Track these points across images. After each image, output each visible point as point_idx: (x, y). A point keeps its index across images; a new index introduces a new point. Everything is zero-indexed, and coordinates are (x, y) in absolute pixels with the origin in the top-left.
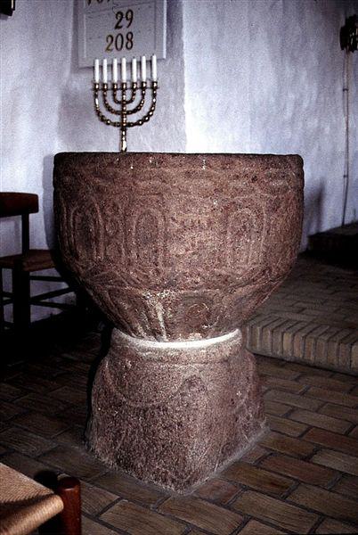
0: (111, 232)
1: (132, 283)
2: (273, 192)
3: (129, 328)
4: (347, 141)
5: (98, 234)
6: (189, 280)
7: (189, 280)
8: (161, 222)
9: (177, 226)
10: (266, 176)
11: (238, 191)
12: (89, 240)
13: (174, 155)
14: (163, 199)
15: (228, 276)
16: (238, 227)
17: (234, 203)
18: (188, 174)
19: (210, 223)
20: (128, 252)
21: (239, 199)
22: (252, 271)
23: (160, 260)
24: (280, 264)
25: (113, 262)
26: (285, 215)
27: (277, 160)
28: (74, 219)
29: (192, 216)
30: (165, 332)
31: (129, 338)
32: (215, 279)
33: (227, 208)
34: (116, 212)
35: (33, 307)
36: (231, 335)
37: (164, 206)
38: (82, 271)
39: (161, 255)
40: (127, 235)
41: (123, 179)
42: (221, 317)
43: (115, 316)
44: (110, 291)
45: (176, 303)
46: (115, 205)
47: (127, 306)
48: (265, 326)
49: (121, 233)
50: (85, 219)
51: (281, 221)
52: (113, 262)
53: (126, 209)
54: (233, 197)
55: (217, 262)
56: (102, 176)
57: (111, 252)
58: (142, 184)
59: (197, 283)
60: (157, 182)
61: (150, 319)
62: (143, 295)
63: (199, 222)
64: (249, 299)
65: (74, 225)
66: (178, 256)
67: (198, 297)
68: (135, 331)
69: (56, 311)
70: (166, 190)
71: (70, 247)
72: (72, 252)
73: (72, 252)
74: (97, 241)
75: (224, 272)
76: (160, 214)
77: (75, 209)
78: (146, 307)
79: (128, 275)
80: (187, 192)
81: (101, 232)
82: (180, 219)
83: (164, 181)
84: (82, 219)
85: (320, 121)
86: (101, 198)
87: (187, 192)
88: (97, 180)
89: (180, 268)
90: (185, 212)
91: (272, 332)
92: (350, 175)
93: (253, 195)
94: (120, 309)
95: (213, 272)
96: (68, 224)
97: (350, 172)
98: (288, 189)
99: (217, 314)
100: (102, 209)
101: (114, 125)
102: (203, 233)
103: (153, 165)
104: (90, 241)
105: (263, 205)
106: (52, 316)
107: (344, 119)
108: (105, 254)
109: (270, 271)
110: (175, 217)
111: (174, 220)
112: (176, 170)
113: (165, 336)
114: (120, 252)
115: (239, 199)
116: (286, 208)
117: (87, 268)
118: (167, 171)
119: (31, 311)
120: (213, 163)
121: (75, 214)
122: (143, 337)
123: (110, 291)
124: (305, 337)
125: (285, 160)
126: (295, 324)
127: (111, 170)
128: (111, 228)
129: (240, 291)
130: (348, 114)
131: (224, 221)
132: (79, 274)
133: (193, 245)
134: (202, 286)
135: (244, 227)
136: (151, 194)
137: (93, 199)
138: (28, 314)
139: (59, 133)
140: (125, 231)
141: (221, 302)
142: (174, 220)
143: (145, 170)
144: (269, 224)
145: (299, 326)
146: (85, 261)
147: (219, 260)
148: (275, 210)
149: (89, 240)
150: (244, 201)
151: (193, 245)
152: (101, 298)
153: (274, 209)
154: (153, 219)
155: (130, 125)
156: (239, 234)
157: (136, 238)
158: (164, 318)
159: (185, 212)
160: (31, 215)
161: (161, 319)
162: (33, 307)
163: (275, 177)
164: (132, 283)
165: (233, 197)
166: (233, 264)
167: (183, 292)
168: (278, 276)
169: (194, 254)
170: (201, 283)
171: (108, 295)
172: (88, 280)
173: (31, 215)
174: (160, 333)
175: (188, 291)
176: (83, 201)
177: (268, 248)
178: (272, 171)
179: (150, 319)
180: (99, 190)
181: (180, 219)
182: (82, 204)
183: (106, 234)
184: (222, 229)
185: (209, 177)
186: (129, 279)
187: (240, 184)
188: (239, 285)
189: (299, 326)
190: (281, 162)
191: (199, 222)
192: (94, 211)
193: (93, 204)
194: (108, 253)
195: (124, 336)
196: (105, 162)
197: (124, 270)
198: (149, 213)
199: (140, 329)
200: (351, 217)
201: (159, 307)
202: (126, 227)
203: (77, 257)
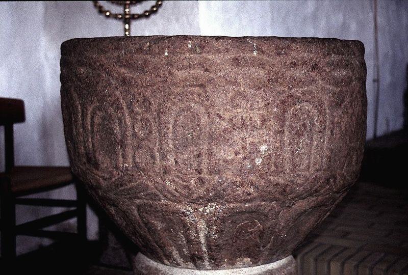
0: (141, 134)
1: (169, 196)
2: (336, 83)
3: (161, 254)
4: (376, 40)
5: (124, 136)
6: (240, 191)
7: (240, 191)
8: (204, 120)
9: (225, 124)
10: (328, 63)
11: (297, 82)
12: (113, 144)
13: (218, 38)
14: (206, 92)
15: (287, 186)
16: (297, 125)
17: (292, 96)
18: (236, 61)
19: (264, 121)
20: (164, 157)
21: (297, 92)
22: (315, 179)
23: (204, 167)
24: (346, 173)
25: (144, 170)
26: (350, 111)
27: (339, 44)
28: (92, 118)
29: (241, 112)
30: (206, 256)
31: (160, 266)
32: (271, 189)
33: (283, 102)
34: (148, 110)
35: (19, 238)
36: (283, 261)
37: (208, 100)
38: (103, 183)
39: (205, 160)
40: (162, 136)
41: (156, 68)
42: (277, 237)
43: (144, 239)
44: (139, 207)
45: (224, 220)
46: (145, 100)
47: (159, 225)
48: (307, 253)
49: (155, 134)
50: (107, 118)
51: (346, 119)
52: (144, 170)
53: (159, 105)
54: (290, 89)
55: (273, 168)
56: (128, 65)
57: (142, 158)
58: (181, 74)
59: (249, 194)
60: (199, 72)
61: (189, 241)
62: (182, 210)
63: (251, 120)
64: (309, 214)
65: (92, 126)
66: (225, 161)
67: (250, 211)
68: (169, 257)
69: (46, 242)
70: (210, 81)
71: (87, 154)
72: (89, 160)
73: (89, 160)
74: (123, 145)
75: (281, 181)
76: (203, 110)
77: (93, 106)
78: (185, 225)
79: (164, 186)
80: (235, 83)
81: (129, 133)
82: (227, 116)
83: (207, 70)
84: (104, 119)
85: (344, 16)
86: (128, 92)
87: (235, 83)
88: (122, 70)
89: (229, 176)
90: (233, 107)
91: (316, 260)
92: (380, 80)
93: (313, 88)
94: (151, 229)
95: (269, 181)
96: (84, 127)
97: (381, 75)
98: (352, 81)
99: (272, 234)
100: (130, 106)
101: (115, 17)
102: (255, 133)
103: (192, 51)
104: (114, 145)
105: (326, 99)
106: (41, 247)
107: (371, 15)
108: (134, 160)
109: (335, 179)
110: (221, 113)
111: (220, 117)
112: (221, 55)
113: (207, 263)
114: (153, 157)
115: (297, 92)
116: (351, 102)
117: (110, 179)
118: (210, 57)
119: (17, 242)
120: (265, 48)
121: (94, 114)
122: (178, 265)
123: (139, 207)
124: (357, 266)
125: (349, 47)
126: (342, 251)
127: (139, 58)
128: (142, 128)
129: (301, 205)
130: (376, 8)
131: (281, 120)
132: (99, 187)
133: (244, 148)
134: (255, 198)
135: (304, 125)
136: (191, 86)
137: (118, 93)
138: (78, 221)
139: (45, 27)
140: (159, 131)
141: (277, 218)
142: (220, 117)
143: (183, 57)
144: (332, 122)
145: (347, 253)
146: (107, 169)
147: (276, 166)
148: (338, 105)
149: (113, 144)
150: (304, 93)
151: (244, 148)
152: (125, 215)
153: (337, 104)
154: (195, 117)
155: (134, 17)
156: (299, 134)
157: (173, 140)
158: (207, 238)
159: (233, 107)
160: (16, 127)
161: (203, 240)
162: (19, 238)
163: (338, 66)
164: (169, 196)
165: (290, 89)
166: (292, 170)
167: (232, 205)
168: (343, 186)
169: (245, 158)
170: (255, 194)
171: (136, 213)
172: (112, 195)
173: (16, 127)
174: (201, 259)
175: (238, 205)
176: (105, 96)
177: (332, 150)
178: (334, 57)
179: (189, 241)
180: (124, 81)
181: (227, 116)
182: (101, 101)
183: (135, 135)
184: (277, 128)
185: (262, 65)
186: (165, 190)
187: (299, 73)
188: (300, 197)
189: (347, 253)
190: (343, 46)
191: (251, 120)
192: (119, 108)
193: (118, 99)
194: (137, 160)
195: (153, 263)
196: (133, 47)
197: (159, 179)
198: (189, 109)
199: (175, 254)
200: (397, 124)
201: (202, 225)
202: (161, 125)
203: (96, 165)
